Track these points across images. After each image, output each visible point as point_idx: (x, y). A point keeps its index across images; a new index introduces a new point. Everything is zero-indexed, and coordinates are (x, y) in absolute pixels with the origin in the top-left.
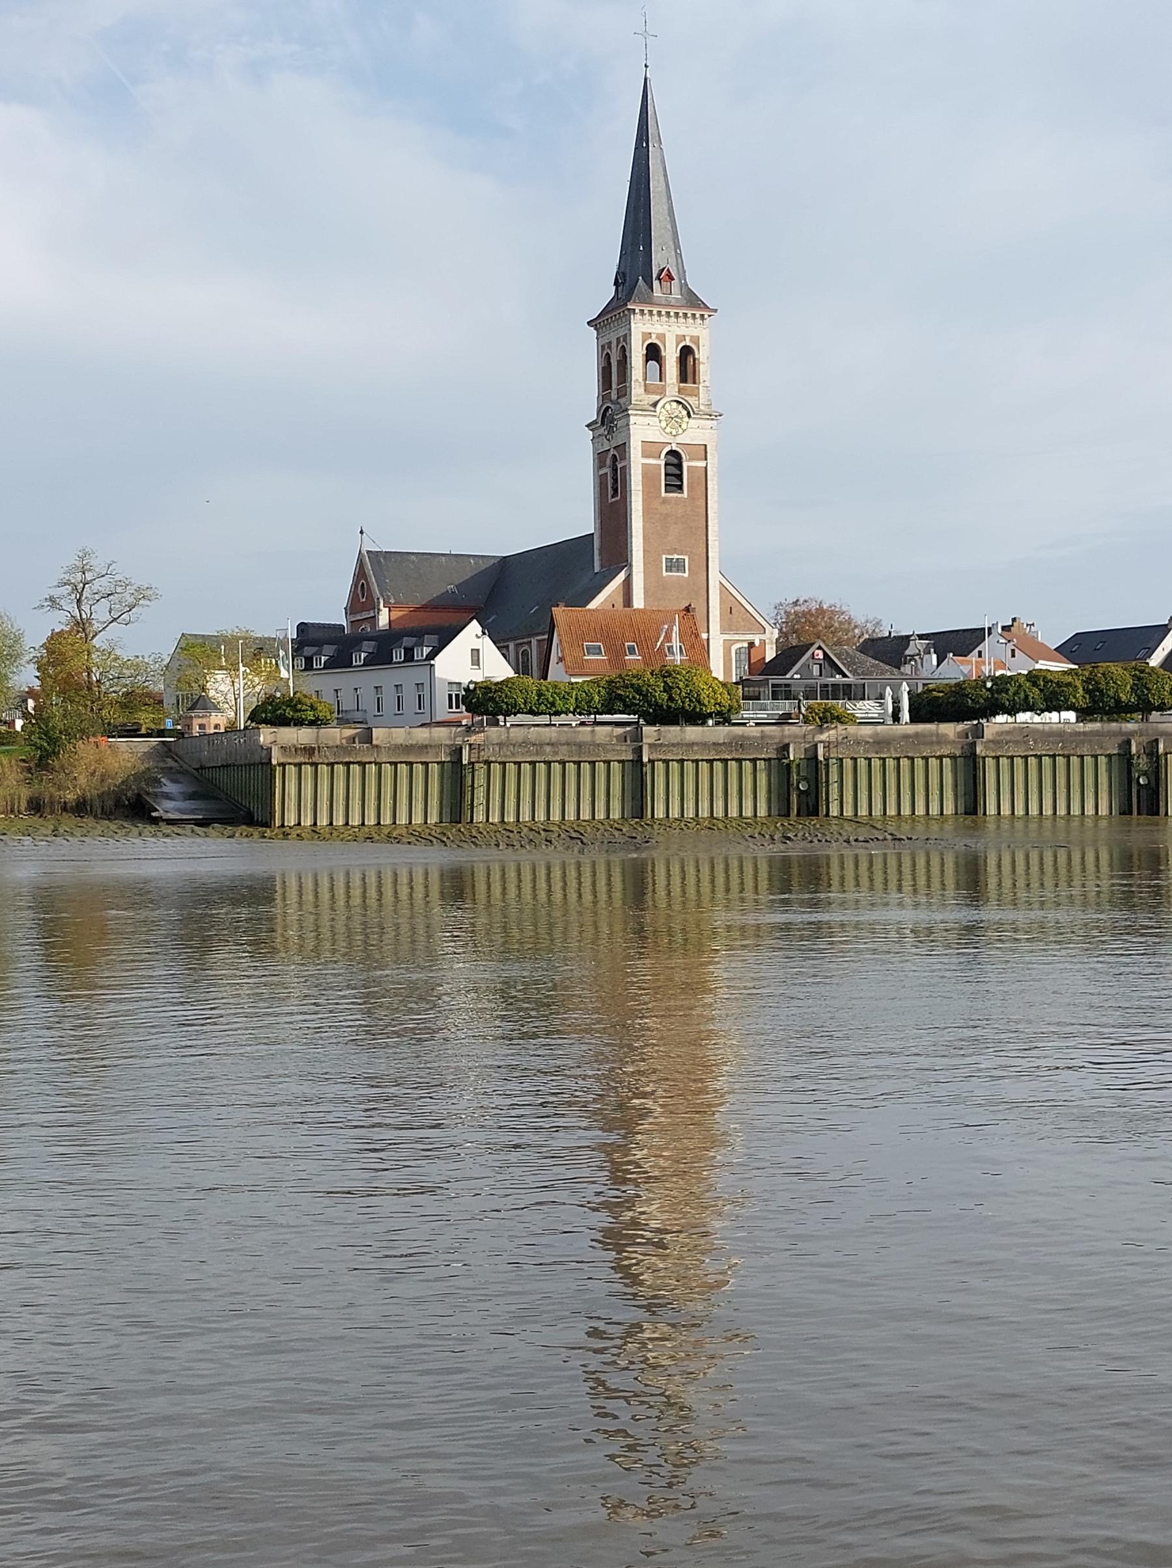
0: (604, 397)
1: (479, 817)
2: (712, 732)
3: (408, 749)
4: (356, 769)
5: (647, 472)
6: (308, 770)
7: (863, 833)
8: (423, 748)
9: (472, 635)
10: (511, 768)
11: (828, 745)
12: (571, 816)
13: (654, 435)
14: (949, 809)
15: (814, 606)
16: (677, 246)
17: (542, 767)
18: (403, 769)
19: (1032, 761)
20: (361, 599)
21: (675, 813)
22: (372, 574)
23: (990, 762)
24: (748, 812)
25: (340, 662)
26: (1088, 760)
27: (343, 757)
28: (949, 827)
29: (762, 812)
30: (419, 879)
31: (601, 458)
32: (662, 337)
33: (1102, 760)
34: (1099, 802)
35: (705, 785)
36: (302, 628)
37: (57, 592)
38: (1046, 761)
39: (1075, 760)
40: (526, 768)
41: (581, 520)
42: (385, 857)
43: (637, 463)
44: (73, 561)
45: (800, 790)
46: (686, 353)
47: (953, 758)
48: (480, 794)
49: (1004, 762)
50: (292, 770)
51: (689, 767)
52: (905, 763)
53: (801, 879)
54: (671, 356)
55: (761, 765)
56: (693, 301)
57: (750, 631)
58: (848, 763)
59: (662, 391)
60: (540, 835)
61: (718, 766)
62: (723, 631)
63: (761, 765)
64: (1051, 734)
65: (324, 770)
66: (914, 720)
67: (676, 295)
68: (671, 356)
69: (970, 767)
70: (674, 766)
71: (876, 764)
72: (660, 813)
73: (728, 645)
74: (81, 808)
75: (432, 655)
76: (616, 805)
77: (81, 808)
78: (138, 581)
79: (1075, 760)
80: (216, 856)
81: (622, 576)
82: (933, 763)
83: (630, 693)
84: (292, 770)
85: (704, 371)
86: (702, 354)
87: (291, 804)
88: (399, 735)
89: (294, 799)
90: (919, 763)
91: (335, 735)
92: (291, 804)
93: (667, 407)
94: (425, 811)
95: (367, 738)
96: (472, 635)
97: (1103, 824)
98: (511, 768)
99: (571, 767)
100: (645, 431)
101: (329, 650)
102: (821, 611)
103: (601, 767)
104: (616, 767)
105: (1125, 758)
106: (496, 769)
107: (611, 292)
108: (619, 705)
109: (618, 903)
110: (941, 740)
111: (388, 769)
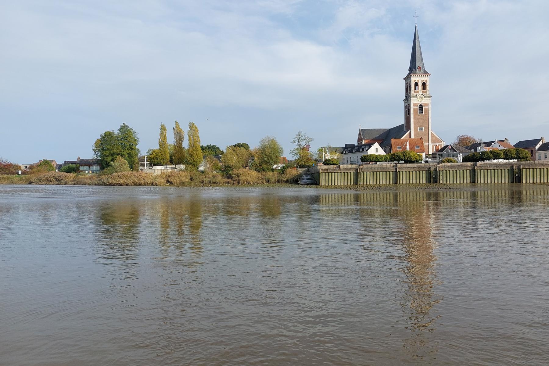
0: (407, 94)
1: (362, 183)
2: (415, 165)
3: (347, 169)
4: (336, 174)
5: (415, 109)
6: (327, 174)
7: (445, 187)
8: (350, 169)
9: (376, 145)
10: (368, 173)
11: (440, 167)
12: (378, 183)
13: (416, 102)
14: (469, 181)
15: (466, 137)
16: (422, 61)
17: (375, 173)
18: (346, 173)
19: (489, 171)
20: (360, 140)
21: (404, 182)
22: (363, 133)
23: (479, 171)
24: (421, 182)
25: (351, 152)
26: (503, 170)
27: (334, 172)
28: (469, 185)
29: (425, 182)
30: (349, 197)
31: (406, 107)
32: (418, 81)
33: (507, 170)
34: (505, 179)
35: (411, 177)
36: (346, 145)
37: (294, 140)
38: (493, 171)
39: (500, 170)
40: (372, 173)
41: (402, 121)
42: (342, 192)
43: (412, 108)
44: (298, 133)
45: (433, 177)
46: (424, 84)
47: (470, 170)
48: (362, 179)
49: (482, 171)
50: (324, 174)
51: (408, 172)
52: (458, 171)
53: (516, 198)
54: (420, 84)
55: (424, 172)
56: (425, 73)
57: (438, 143)
58: (445, 171)
59: (418, 92)
60: (372, 187)
61: (414, 172)
62: (432, 142)
63: (424, 172)
64: (494, 164)
65: (330, 174)
66: (463, 161)
67: (422, 71)
68: (420, 84)
69: (474, 173)
70: (404, 172)
71: (451, 171)
72: (401, 182)
73: (433, 146)
74: (286, 182)
75: (367, 150)
76: (391, 181)
77: (286, 182)
78: (310, 137)
79: (500, 170)
80: (311, 191)
81: (409, 132)
82: (465, 171)
83: (396, 157)
84: (324, 174)
85: (428, 87)
86: (427, 84)
87: (324, 181)
88: (345, 166)
89: (324, 180)
90: (461, 171)
91: (333, 167)
92: (324, 181)
93: (419, 95)
94: (350, 182)
95: (339, 167)
96: (376, 145)
97: (507, 185)
98: (368, 173)
99: (381, 173)
100: (414, 100)
101: (349, 149)
102: (468, 138)
103: (388, 173)
104: (391, 173)
105: (512, 169)
106: (365, 173)
107: (408, 72)
108: (393, 159)
109: (392, 202)
110: (467, 166)
111: (343, 173)
